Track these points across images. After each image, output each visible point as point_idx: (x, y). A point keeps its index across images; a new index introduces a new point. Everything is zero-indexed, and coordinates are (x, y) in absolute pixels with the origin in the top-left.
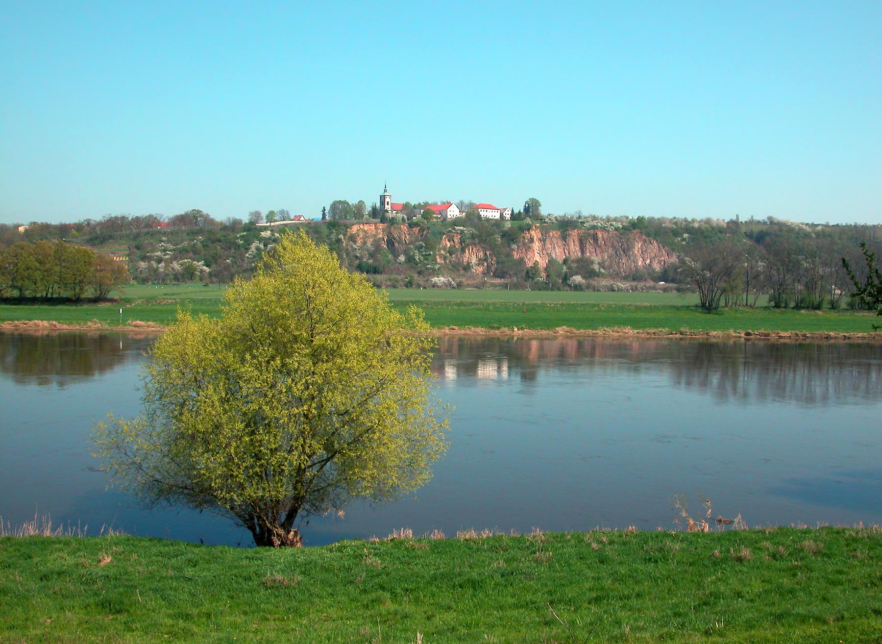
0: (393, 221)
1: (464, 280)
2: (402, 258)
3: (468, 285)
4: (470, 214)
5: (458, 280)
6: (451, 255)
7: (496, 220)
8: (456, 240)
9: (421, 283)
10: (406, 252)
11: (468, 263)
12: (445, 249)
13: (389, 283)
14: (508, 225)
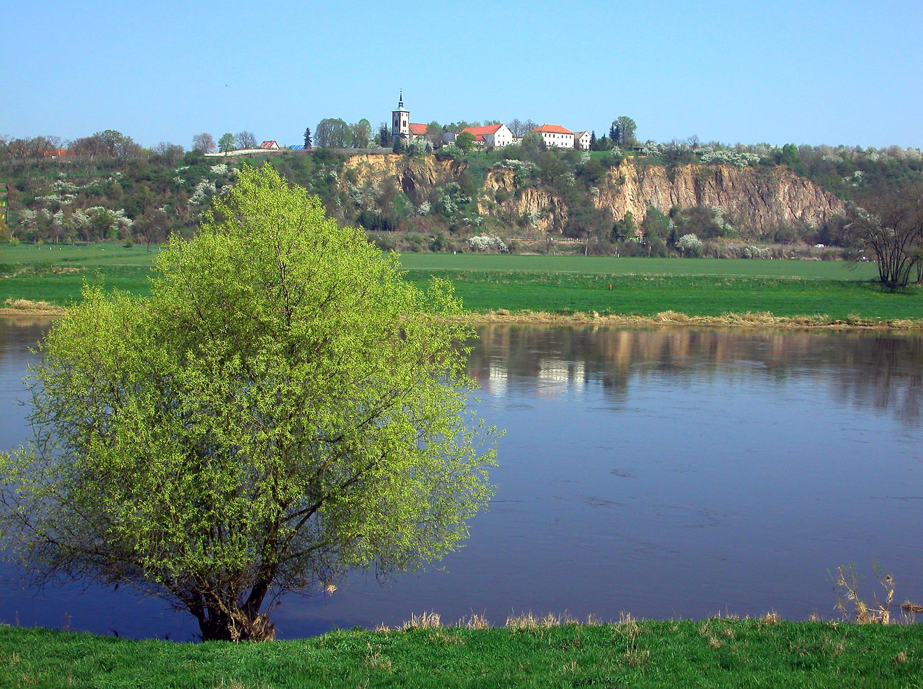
0: (411, 151)
3: (525, 248)
5: (510, 240)
6: (499, 202)
7: (569, 150)
8: (507, 180)
10: (432, 199)
11: (526, 215)
12: (490, 193)
13: (406, 244)
14: (586, 157)
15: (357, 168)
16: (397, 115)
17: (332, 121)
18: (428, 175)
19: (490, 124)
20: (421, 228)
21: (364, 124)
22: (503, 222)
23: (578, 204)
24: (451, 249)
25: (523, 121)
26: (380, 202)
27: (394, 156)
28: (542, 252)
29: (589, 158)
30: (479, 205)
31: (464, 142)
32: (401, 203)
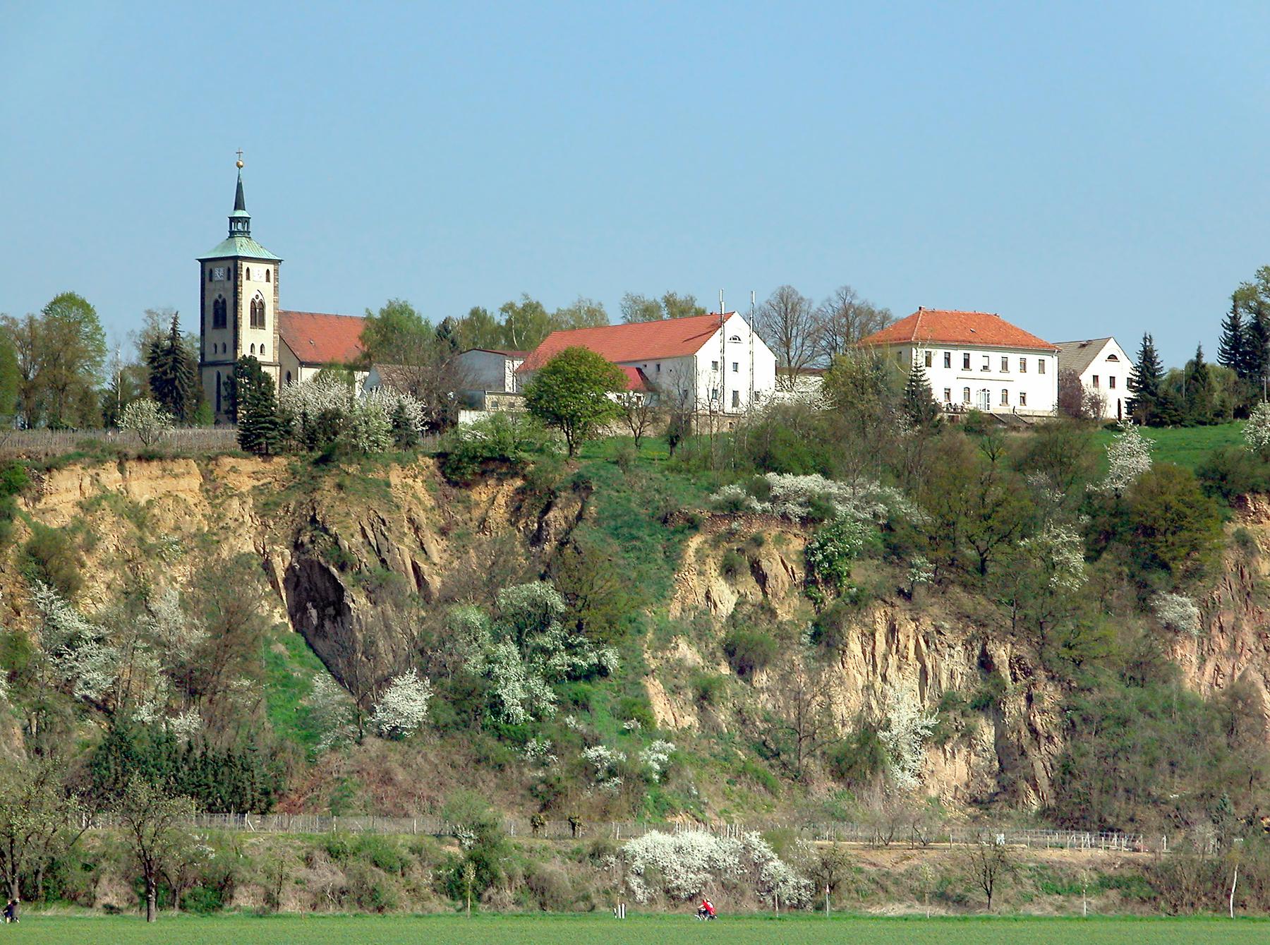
0: (326, 440)
1: (848, 847)
2: (408, 699)
3: (883, 886)
4: (859, 385)
5: (812, 848)
6: (743, 670)
7: (1044, 427)
8: (773, 567)
9: (557, 869)
10: (426, 658)
11: (868, 732)
12: (699, 630)
13: (329, 875)
14: (1132, 457)
15: (78, 525)
16: (219, 283)
17: (83, 305)
18: (404, 553)
19: (649, 311)
20: (390, 798)
21: (70, 315)
22: (762, 765)
23: (1108, 677)
24: (540, 893)
25: (819, 296)
26: (190, 683)
27: (250, 465)
28: (960, 901)
29: (1144, 462)
30: (654, 688)
31: (561, 397)
32: (286, 682)
